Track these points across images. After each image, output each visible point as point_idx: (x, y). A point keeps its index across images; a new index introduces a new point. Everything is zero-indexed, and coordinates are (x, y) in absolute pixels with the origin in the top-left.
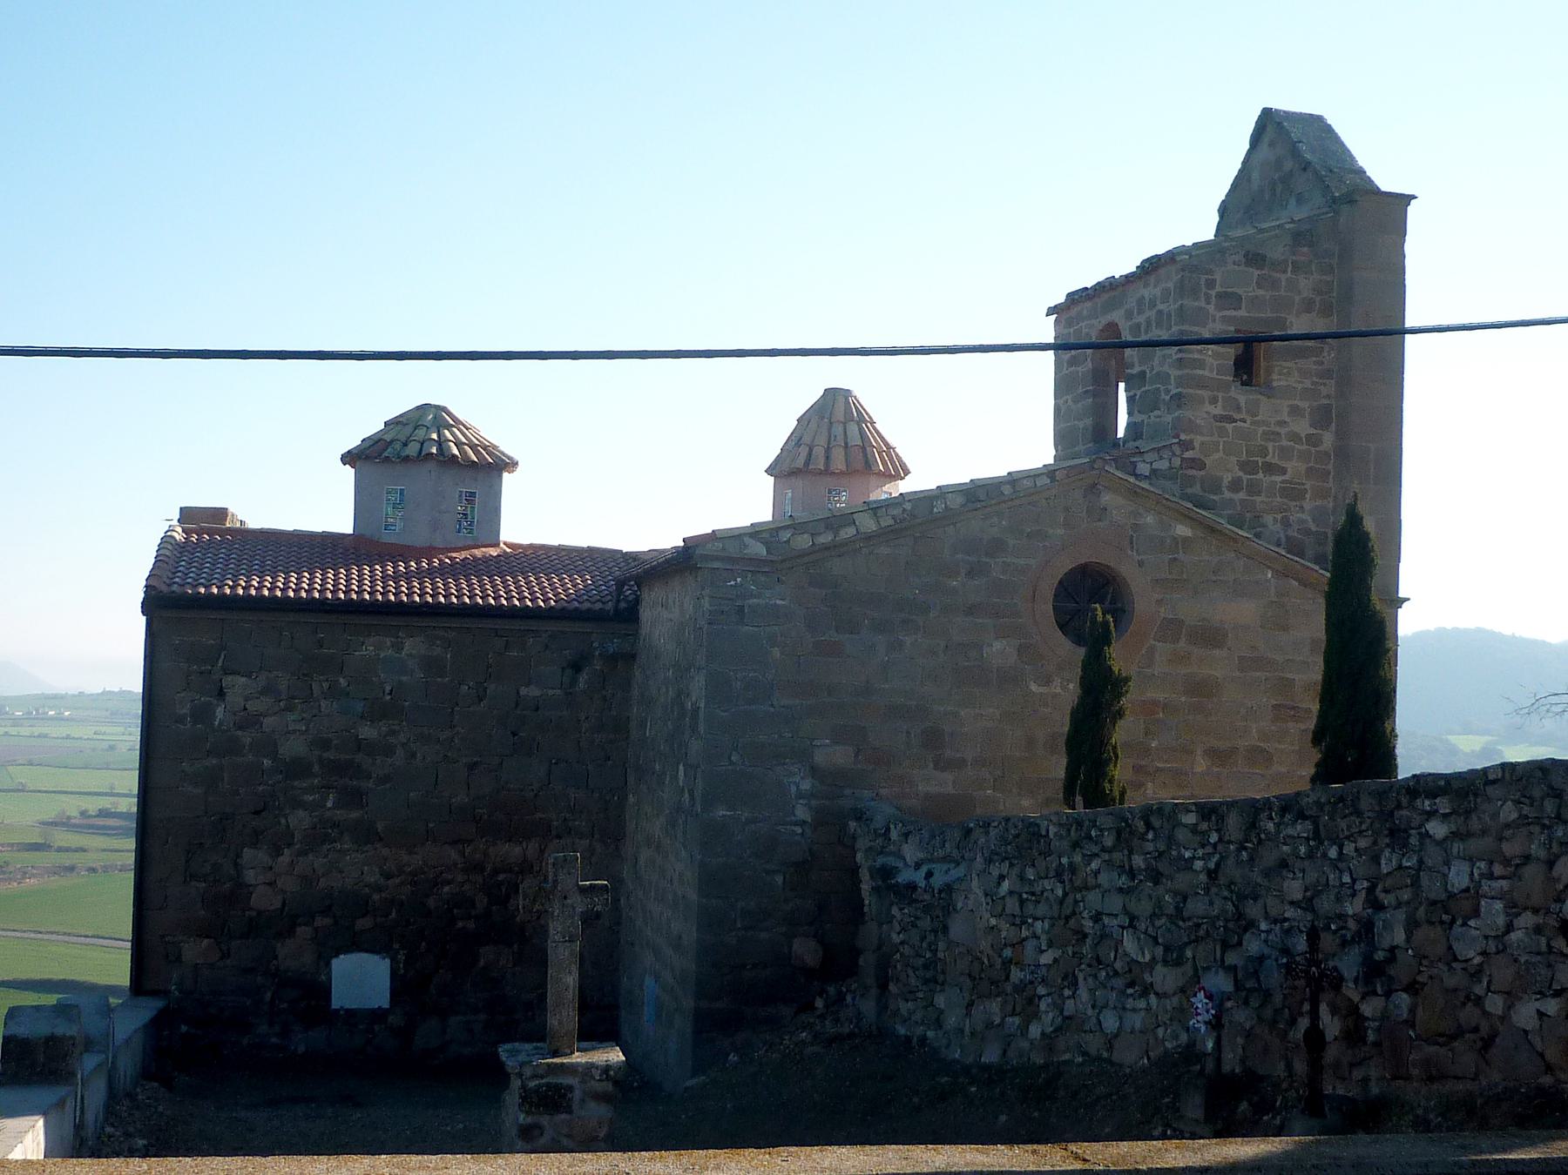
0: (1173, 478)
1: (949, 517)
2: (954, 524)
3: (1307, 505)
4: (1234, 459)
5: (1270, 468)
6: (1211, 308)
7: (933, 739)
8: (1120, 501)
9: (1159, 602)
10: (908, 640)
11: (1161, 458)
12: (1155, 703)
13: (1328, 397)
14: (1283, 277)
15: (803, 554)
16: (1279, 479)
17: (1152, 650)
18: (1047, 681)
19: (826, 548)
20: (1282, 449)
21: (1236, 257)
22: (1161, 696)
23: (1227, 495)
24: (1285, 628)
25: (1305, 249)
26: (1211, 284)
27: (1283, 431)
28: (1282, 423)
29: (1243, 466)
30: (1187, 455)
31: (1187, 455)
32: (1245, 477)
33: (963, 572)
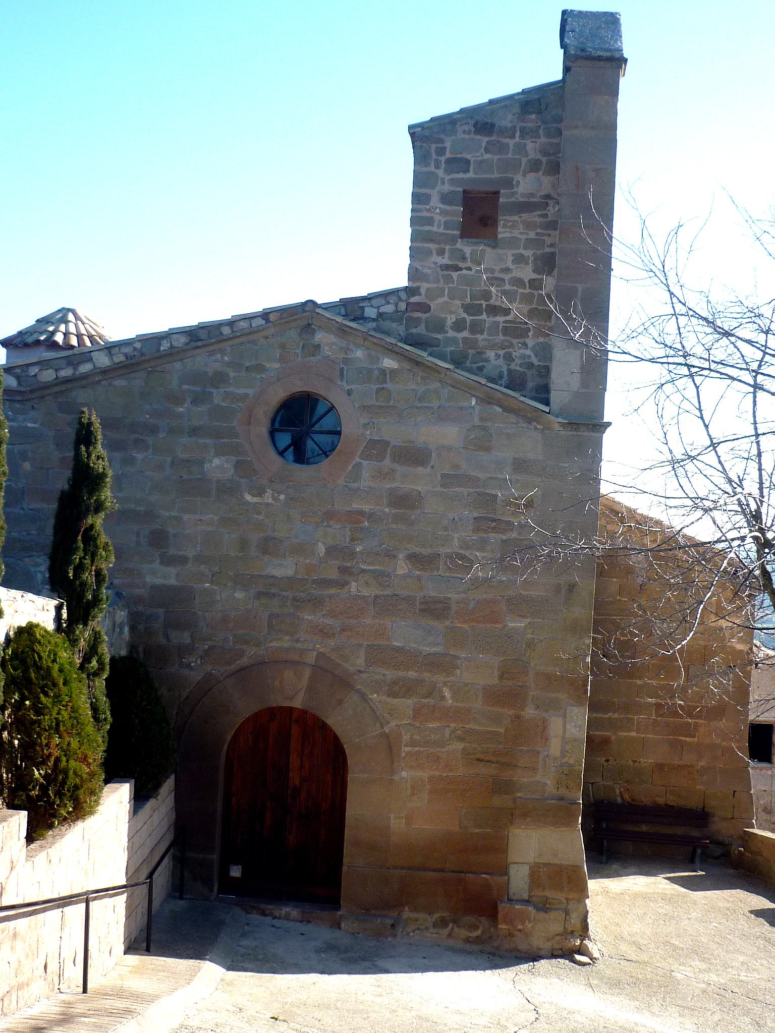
0: (399, 320)
1: (174, 354)
2: (181, 360)
3: (530, 342)
4: (458, 303)
5: (494, 310)
6: (441, 173)
7: (159, 539)
8: (332, 338)
9: (366, 426)
10: (139, 456)
11: (388, 303)
12: (361, 513)
13: (552, 245)
14: (511, 143)
15: (47, 386)
16: (500, 319)
17: (359, 465)
18: (260, 493)
19: (67, 381)
20: (504, 293)
21: (466, 127)
22: (366, 508)
23: (451, 334)
24: (488, 449)
25: (533, 116)
26: (441, 151)
27: (507, 277)
28: (507, 270)
29: (467, 308)
30: (413, 300)
31: (413, 300)
32: (469, 319)
33: (189, 400)
